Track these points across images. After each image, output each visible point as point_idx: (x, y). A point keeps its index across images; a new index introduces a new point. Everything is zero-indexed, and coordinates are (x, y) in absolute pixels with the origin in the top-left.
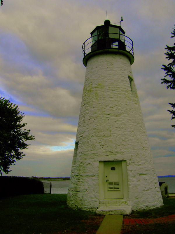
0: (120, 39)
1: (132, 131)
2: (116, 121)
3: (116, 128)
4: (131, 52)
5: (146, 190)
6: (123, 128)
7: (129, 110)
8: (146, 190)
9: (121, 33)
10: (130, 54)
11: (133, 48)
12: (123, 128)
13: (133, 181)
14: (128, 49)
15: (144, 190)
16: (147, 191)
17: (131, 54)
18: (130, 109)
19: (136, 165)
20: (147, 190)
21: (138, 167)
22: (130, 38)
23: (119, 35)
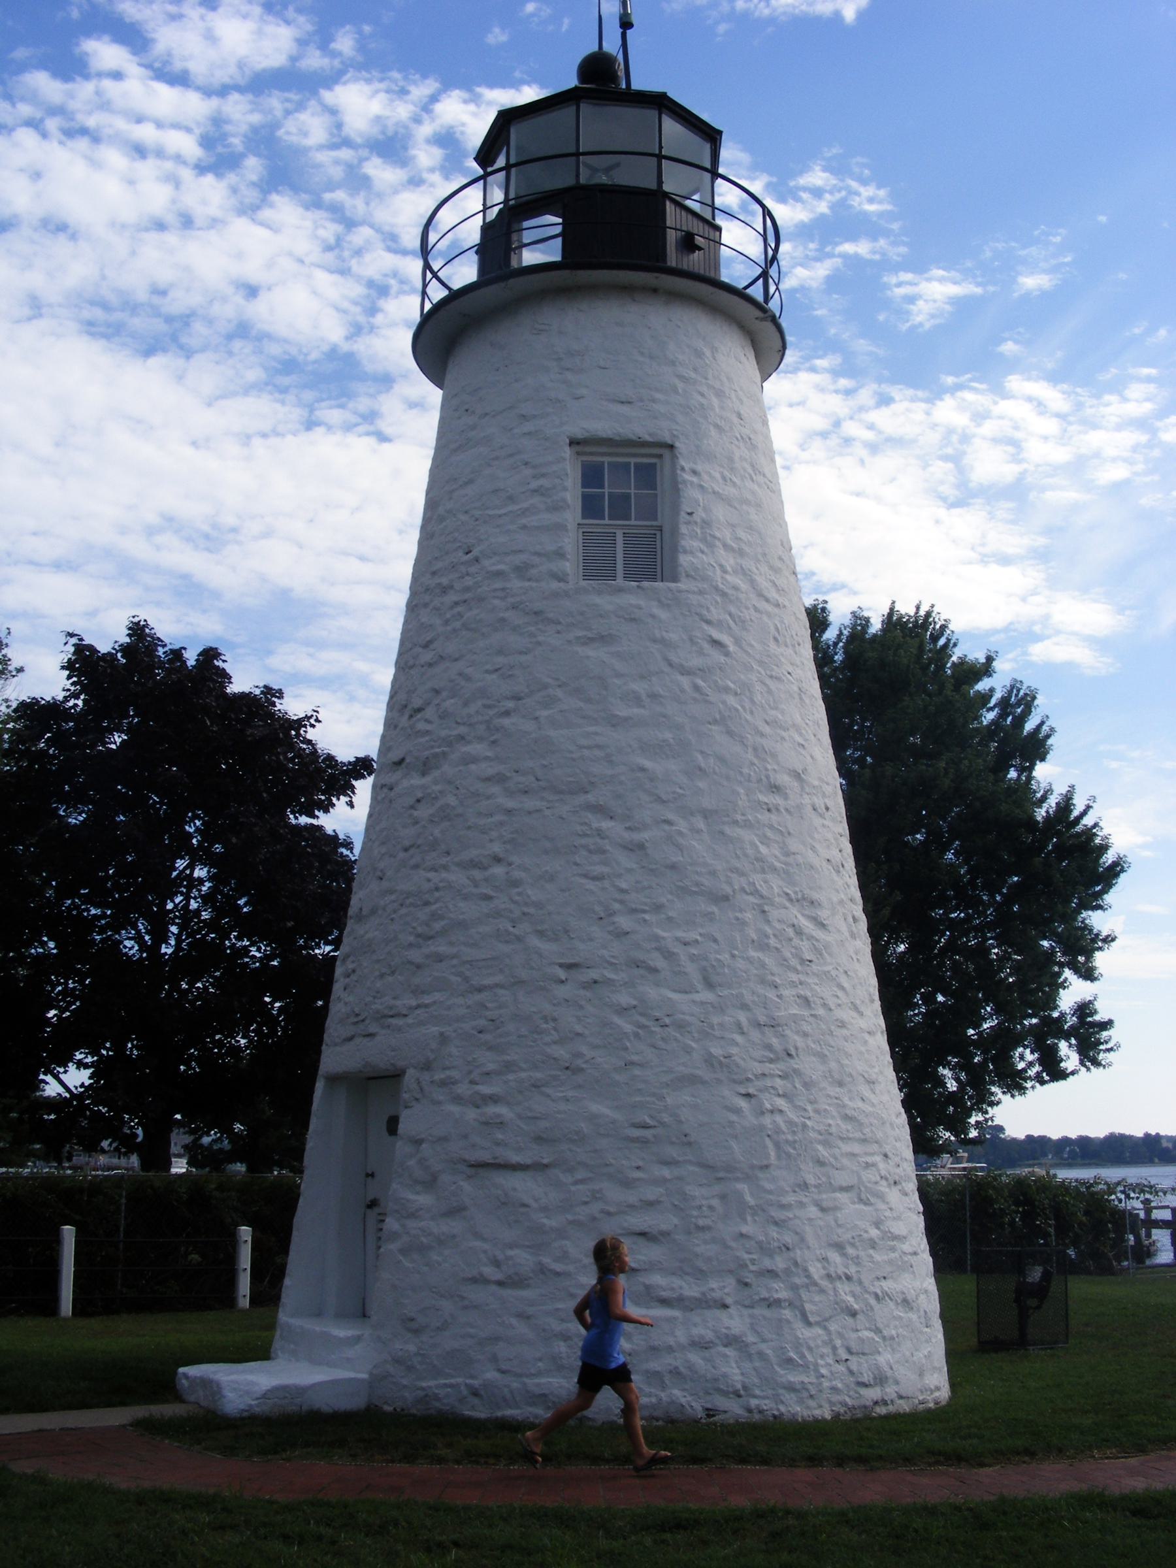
2: (411, 801)
3: (406, 850)
4: (756, 292)
5: (500, 1283)
7: (510, 704)
8: (500, 1283)
13: (413, 1215)
15: (474, 1280)
16: (507, 1293)
19: (458, 1099)
20: (515, 1281)
21: (471, 1114)
22: (645, 151)
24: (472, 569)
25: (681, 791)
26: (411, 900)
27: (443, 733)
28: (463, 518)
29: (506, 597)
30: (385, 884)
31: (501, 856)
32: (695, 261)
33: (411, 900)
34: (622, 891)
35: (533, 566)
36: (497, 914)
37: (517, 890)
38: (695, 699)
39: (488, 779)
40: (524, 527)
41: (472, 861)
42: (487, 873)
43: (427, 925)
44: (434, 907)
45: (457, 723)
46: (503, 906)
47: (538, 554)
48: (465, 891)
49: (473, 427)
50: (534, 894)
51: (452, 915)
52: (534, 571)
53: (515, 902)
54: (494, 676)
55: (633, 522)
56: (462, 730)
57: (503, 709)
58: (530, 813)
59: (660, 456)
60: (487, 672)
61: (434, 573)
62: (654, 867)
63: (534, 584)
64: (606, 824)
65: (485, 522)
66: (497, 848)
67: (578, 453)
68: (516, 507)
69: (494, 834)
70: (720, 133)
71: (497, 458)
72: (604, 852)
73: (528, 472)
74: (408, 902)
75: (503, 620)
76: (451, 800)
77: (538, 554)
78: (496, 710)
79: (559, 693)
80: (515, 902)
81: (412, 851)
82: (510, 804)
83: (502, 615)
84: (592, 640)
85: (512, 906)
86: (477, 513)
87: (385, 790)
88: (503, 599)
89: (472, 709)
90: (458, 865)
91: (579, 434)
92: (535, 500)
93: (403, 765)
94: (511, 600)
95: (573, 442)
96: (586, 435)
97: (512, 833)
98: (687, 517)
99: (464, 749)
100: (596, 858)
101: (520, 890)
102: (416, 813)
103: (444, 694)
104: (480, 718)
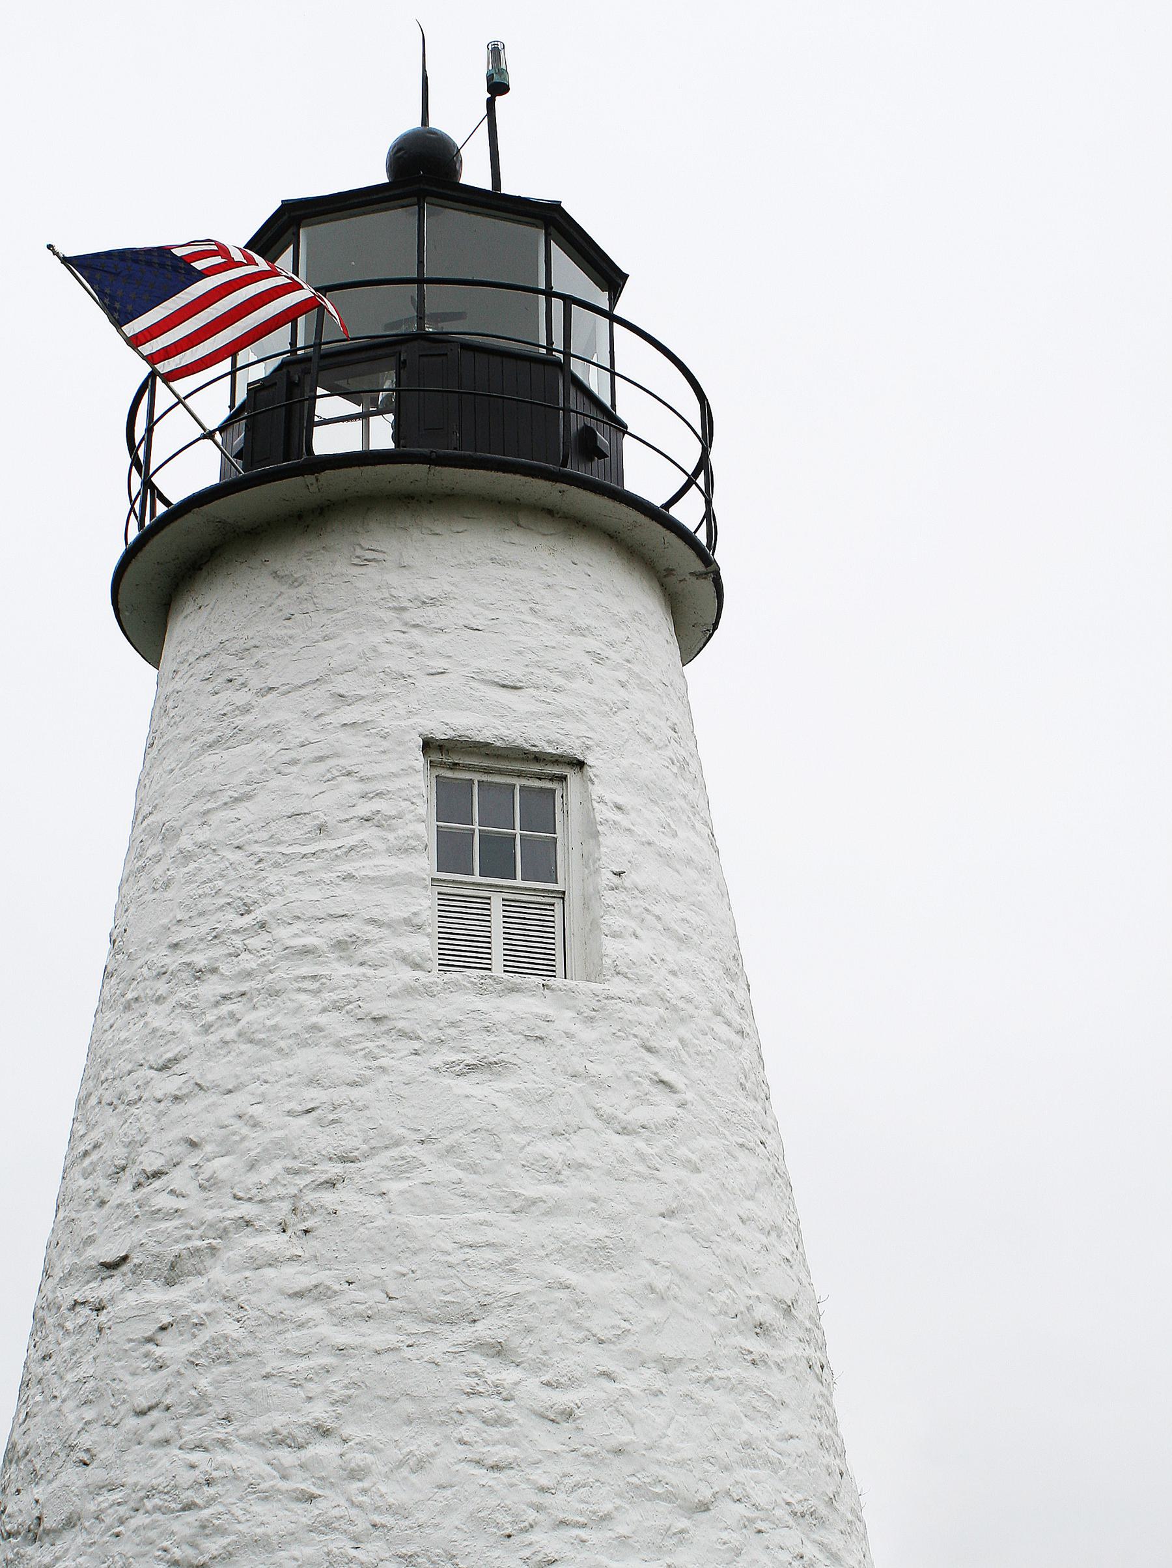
0: (567, 354)
1: (301, 1435)
2: (150, 1329)
3: (142, 1413)
4: (688, 512)
6: (198, 1406)
7: (335, 1169)
9: (569, 276)
10: (671, 537)
11: (704, 464)
12: (198, 1406)
14: (646, 476)
17: (686, 537)
18: (344, 1159)
23: (542, 298)
24: (255, 942)
25: (626, 1325)
26: (157, 1501)
27: (210, 1215)
28: (237, 856)
29: (319, 991)
30: (94, 1474)
31: (329, 1424)
32: (593, 471)
33: (157, 1501)
34: (543, 1490)
35: (367, 941)
36: (329, 1526)
37: (360, 1484)
38: (639, 1175)
39: (299, 1295)
40: (350, 877)
41: (275, 1432)
42: (305, 1454)
43: (194, 1545)
44: (205, 1513)
45: (235, 1197)
46: (336, 1512)
47: (373, 921)
48: (264, 1486)
49: (246, 710)
50: (393, 1492)
51: (240, 1527)
52: (368, 952)
53: (360, 1506)
54: (305, 1120)
55: (519, 882)
56: (246, 1210)
57: (324, 1177)
58: (378, 1353)
59: (562, 779)
60: (290, 1113)
61: (175, 946)
62: (591, 1450)
63: (370, 972)
64: (509, 1376)
65: (276, 865)
66: (319, 1411)
67: (433, 765)
68: (334, 844)
69: (313, 1388)
70: (625, 277)
71: (294, 762)
72: (509, 1423)
73: (351, 787)
74: (149, 1504)
75: (316, 1028)
76: (231, 1329)
77: (373, 921)
78: (308, 1179)
79: (422, 1154)
80: (360, 1506)
81: (154, 1415)
82: (342, 1337)
83: (314, 1019)
84: (471, 1068)
85: (353, 1512)
86: (260, 850)
87: (85, 1311)
88: (316, 993)
89: (266, 1173)
90: (246, 1439)
91: (441, 733)
92: (367, 833)
93: (124, 1268)
94: (327, 995)
95: (428, 745)
96: (451, 734)
97: (346, 1387)
98: (615, 879)
99: (251, 1242)
100: (495, 1433)
101: (366, 1484)
102: (158, 1351)
103: (209, 1148)
104: (282, 1191)
